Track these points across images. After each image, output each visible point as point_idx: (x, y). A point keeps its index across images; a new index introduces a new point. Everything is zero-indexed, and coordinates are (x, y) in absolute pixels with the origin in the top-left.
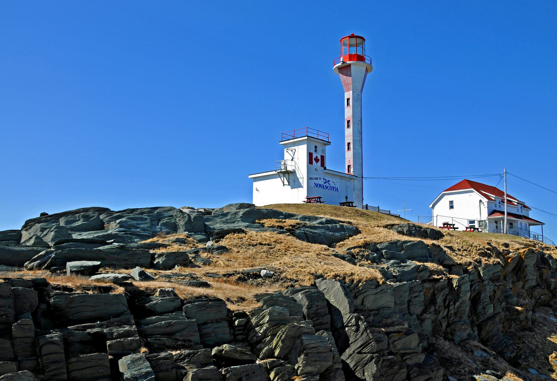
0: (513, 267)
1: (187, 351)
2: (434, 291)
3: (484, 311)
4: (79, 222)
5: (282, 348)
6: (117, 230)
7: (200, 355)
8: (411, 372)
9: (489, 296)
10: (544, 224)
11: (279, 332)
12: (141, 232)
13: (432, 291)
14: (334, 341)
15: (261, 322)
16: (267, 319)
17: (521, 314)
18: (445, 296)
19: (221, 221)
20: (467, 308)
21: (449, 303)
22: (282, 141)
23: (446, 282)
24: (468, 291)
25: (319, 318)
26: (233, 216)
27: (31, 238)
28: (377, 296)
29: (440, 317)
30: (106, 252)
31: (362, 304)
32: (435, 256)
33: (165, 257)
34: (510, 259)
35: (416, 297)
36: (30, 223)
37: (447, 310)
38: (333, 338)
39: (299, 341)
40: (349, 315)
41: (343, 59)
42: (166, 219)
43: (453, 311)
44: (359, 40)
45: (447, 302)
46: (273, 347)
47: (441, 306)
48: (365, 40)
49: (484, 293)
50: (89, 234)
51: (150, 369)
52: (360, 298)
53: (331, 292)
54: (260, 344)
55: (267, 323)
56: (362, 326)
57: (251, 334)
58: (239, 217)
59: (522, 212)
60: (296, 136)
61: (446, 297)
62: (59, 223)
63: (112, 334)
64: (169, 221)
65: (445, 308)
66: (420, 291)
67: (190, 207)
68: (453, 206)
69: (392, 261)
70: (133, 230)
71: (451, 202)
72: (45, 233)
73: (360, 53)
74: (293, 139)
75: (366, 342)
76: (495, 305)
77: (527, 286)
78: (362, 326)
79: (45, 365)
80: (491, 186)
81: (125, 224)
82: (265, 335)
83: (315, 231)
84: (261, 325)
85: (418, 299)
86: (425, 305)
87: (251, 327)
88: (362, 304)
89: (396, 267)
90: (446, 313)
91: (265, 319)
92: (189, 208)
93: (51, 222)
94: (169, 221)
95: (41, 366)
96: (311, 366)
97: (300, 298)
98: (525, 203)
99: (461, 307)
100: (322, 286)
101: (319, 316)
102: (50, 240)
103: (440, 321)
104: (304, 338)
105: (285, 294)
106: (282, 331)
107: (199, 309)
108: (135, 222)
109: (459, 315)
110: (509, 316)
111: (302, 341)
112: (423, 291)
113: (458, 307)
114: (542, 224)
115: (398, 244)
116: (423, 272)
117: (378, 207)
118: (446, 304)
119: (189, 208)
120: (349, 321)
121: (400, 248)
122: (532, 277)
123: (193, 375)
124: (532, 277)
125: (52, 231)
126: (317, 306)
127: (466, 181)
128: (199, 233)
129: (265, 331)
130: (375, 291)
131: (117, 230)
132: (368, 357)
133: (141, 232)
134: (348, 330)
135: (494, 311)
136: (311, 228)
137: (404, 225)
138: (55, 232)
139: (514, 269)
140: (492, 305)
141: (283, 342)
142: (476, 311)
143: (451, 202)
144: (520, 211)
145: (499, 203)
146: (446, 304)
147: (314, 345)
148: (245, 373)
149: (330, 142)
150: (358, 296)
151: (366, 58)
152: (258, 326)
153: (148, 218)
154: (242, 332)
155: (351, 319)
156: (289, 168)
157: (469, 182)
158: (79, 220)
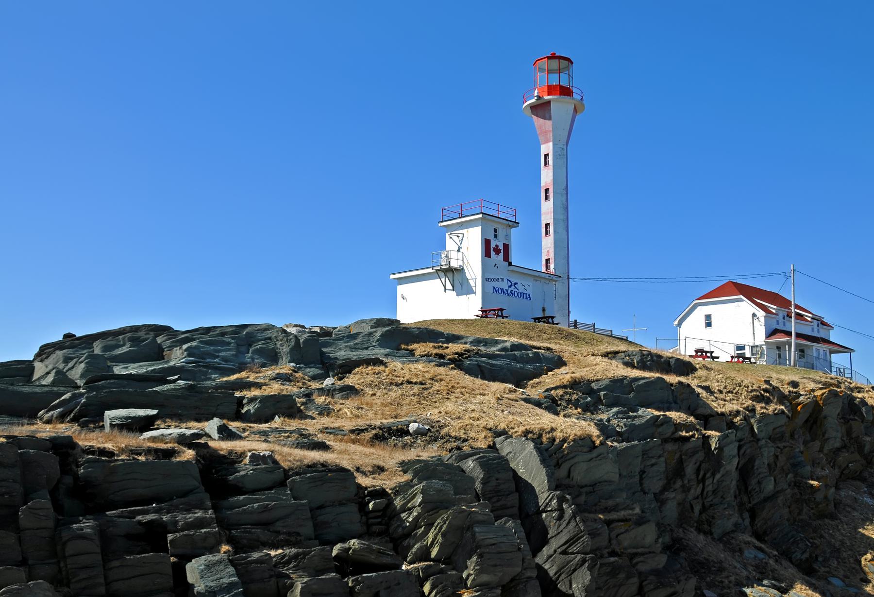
0: (805, 419)
3: (760, 487)
4: (124, 348)
5: (442, 546)
8: (644, 583)
9: (768, 464)
10: (853, 351)
11: (438, 521)
12: (221, 364)
13: (677, 456)
16: (420, 500)
18: (698, 464)
21: (705, 475)
23: (700, 443)
24: (734, 457)
25: (500, 498)
26: (366, 339)
27: (48, 373)
33: (259, 402)
34: (801, 406)
35: (652, 465)
36: (47, 349)
37: (701, 485)
39: (469, 534)
40: (548, 494)
41: (538, 93)
42: (261, 342)
44: (564, 63)
45: (702, 473)
46: (429, 544)
48: (573, 63)
50: (140, 366)
52: (565, 467)
53: (520, 457)
55: (419, 506)
56: (569, 510)
58: (376, 340)
64: (265, 346)
65: (698, 482)
66: (660, 457)
67: (298, 324)
70: (208, 360)
71: (708, 317)
72: (70, 365)
73: (564, 83)
74: (460, 218)
75: (574, 536)
78: (569, 510)
82: (416, 524)
83: (494, 362)
84: (410, 509)
87: (393, 513)
89: (621, 418)
90: (699, 490)
91: (415, 499)
92: (296, 326)
93: (80, 348)
94: (265, 346)
97: (471, 467)
98: (823, 318)
99: (723, 481)
101: (500, 496)
102: (78, 376)
104: (477, 530)
108: (212, 348)
112: (663, 456)
113: (718, 481)
114: (850, 350)
116: (664, 426)
117: (594, 325)
118: (701, 476)
119: (296, 326)
120: (548, 504)
122: (835, 434)
127: (731, 284)
128: (313, 365)
129: (416, 519)
132: (577, 559)
133: (221, 364)
134: (547, 516)
135: (775, 487)
141: (443, 535)
143: (708, 317)
146: (701, 476)
147: (492, 541)
151: (575, 90)
153: (233, 341)
154: (379, 520)
155: (551, 500)
156: (454, 264)
157: (735, 284)
158: (124, 345)
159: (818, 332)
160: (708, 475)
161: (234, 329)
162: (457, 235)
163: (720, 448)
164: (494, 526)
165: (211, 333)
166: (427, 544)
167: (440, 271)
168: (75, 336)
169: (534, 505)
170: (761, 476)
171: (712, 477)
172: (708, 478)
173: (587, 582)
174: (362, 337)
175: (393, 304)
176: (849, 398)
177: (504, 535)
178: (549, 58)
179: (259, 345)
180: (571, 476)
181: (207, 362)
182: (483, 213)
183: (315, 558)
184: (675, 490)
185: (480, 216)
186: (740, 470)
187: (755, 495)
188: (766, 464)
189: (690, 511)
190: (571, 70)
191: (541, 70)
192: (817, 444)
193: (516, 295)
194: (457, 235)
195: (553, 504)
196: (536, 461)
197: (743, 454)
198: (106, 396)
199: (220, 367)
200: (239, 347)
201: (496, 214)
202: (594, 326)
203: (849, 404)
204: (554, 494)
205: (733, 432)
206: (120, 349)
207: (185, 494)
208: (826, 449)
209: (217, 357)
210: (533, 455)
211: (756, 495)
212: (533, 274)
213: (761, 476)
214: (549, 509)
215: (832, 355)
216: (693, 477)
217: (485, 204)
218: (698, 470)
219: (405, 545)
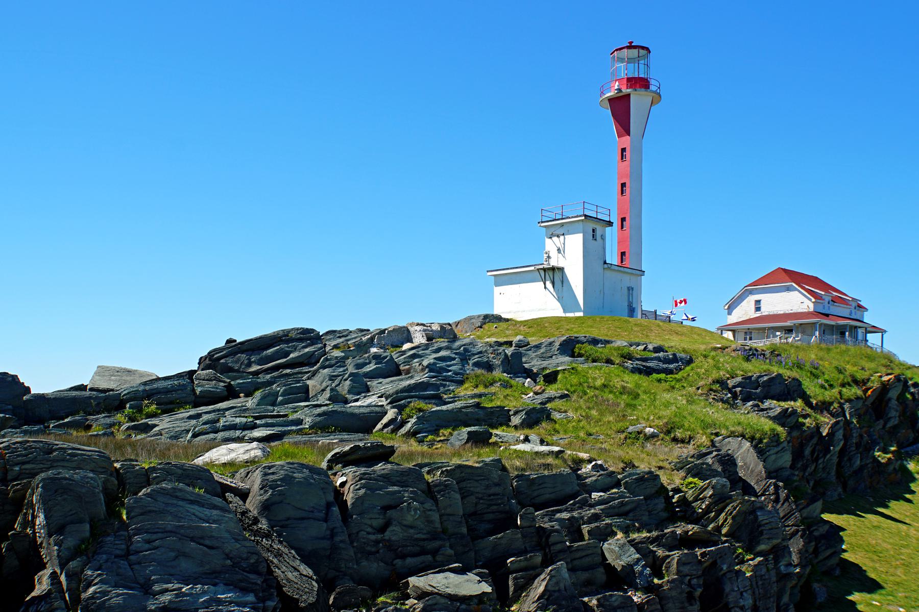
1: (654, 533)
2: (802, 440)
4: (371, 365)
5: (731, 526)
6: (426, 375)
7: (668, 537)
8: (819, 545)
10: (885, 331)
13: (799, 440)
16: (710, 493)
18: (813, 447)
19: (536, 355)
20: (835, 460)
21: (818, 455)
22: (542, 222)
23: (815, 430)
24: (841, 440)
26: (549, 348)
27: (323, 390)
28: (779, 455)
29: (807, 474)
30: (467, 414)
32: (794, 391)
33: (525, 414)
34: (871, 390)
36: (216, 354)
37: (815, 464)
39: (752, 517)
40: (765, 482)
41: (618, 86)
42: (476, 356)
43: (821, 466)
44: (642, 52)
48: (650, 52)
50: (392, 382)
51: (638, 556)
53: (738, 454)
55: (710, 497)
56: (783, 494)
58: (556, 349)
59: (855, 314)
60: (566, 214)
61: (815, 447)
62: (346, 368)
63: (582, 518)
64: (480, 359)
67: (420, 322)
68: (760, 307)
69: (751, 403)
71: (758, 302)
72: (336, 382)
74: (562, 219)
75: (788, 513)
78: (783, 494)
79: (553, 555)
80: (812, 276)
81: (434, 367)
82: (708, 510)
83: (648, 364)
84: (701, 499)
90: (813, 468)
92: (418, 324)
93: (338, 367)
94: (480, 359)
95: (549, 557)
96: (765, 544)
98: (860, 301)
99: (831, 460)
102: (346, 392)
104: (759, 514)
105: (123, 396)
107: (637, 484)
108: (444, 364)
109: (828, 470)
111: (756, 517)
113: (827, 460)
114: (883, 332)
115: (753, 379)
116: (792, 417)
117: (655, 312)
119: (418, 324)
120: (766, 489)
121: (756, 385)
122: (894, 414)
123: (678, 560)
124: (894, 414)
125: (346, 380)
128: (520, 375)
129: (708, 507)
130: (776, 450)
131: (426, 375)
132: (792, 530)
133: (454, 377)
134: (765, 499)
136: (644, 361)
137: (738, 349)
138: (350, 380)
141: (733, 518)
143: (758, 302)
144: (826, 308)
145: (829, 303)
147: (768, 521)
148: (719, 555)
151: (652, 82)
152: (697, 501)
153: (456, 356)
155: (768, 487)
157: (785, 271)
158: (370, 363)
159: (855, 314)
160: (821, 455)
163: (831, 434)
165: (430, 349)
168: (235, 341)
170: (852, 453)
173: (800, 546)
174: (546, 346)
175: (491, 303)
178: (628, 47)
179: (476, 359)
182: (586, 216)
183: (669, 538)
184: (798, 469)
185: (583, 218)
191: (621, 60)
192: (882, 422)
198: (429, 416)
202: (656, 313)
204: (771, 483)
205: (842, 420)
206: (368, 366)
207: (573, 496)
208: (889, 425)
209: (450, 371)
213: (852, 453)
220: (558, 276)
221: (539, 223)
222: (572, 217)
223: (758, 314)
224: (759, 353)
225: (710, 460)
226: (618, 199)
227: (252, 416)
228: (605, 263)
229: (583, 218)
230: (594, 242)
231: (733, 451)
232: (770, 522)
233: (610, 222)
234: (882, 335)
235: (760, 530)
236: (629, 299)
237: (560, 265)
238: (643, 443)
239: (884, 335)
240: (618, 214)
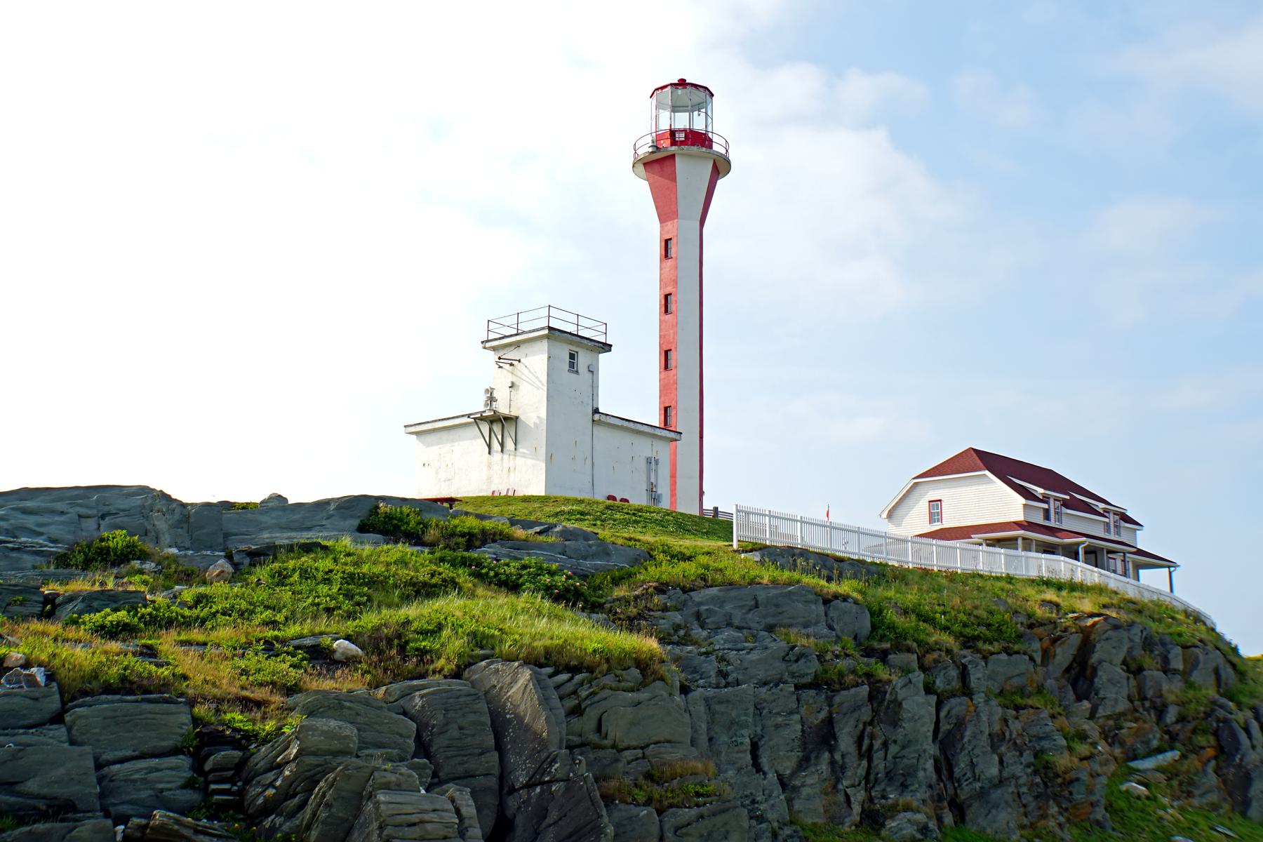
0: (1065, 665)
3: (974, 772)
9: (990, 735)
11: (322, 784)
12: (46, 546)
14: (475, 811)
15: (278, 760)
16: (295, 751)
17: (1076, 784)
25: (465, 759)
31: (599, 729)
35: (777, 727)
37: (865, 763)
38: (471, 802)
45: (866, 742)
46: (304, 823)
47: (847, 753)
49: (975, 725)
52: (591, 715)
54: (273, 816)
57: (251, 790)
60: (523, 327)
65: (861, 756)
66: (792, 713)
70: (23, 539)
71: (935, 503)
73: (699, 125)
76: (1004, 759)
77: (1101, 712)
85: (785, 732)
86: (804, 746)
87: (252, 773)
88: (599, 729)
89: (729, 649)
91: (289, 750)
97: (417, 707)
100: (488, 673)
101: (466, 756)
103: (846, 792)
106: (326, 781)
110: (1042, 786)
112: (797, 713)
113: (894, 758)
114: (1169, 564)
118: (864, 748)
126: (461, 728)
127: (972, 452)
133: (46, 546)
135: (1000, 771)
139: (1068, 670)
140: (996, 758)
142: (951, 772)
143: (935, 503)
146: (864, 748)
147: (414, 819)
149: (611, 346)
150: (586, 708)
151: (715, 138)
154: (227, 786)
156: (503, 410)
161: (82, 492)
162: (510, 362)
164: (419, 794)
166: (302, 824)
167: (481, 420)
169: (524, 773)
171: (884, 750)
172: (877, 751)
176: (1145, 633)
177: (434, 810)
180: (604, 729)
181: (21, 543)
182: (550, 328)
186: (941, 742)
187: (965, 783)
188: (987, 733)
189: (845, 805)
190: (709, 107)
193: (1063, 694)
194: (510, 362)
195: (553, 770)
196: (532, 699)
197: (946, 716)
199: (43, 551)
200: (82, 519)
201: (572, 329)
203: (1144, 643)
210: (528, 690)
211: (967, 785)
212: (633, 427)
214: (546, 779)
215: (1141, 571)
216: (852, 749)
217: (582, 321)
218: (860, 741)
219: (267, 826)
220: (510, 429)
221: (482, 342)
222: (530, 332)
223: (936, 526)
224: (601, 507)
225: (417, 700)
226: (661, 321)
227: (1167, 812)
228: (596, 411)
229: (546, 332)
230: (574, 376)
231: (501, 688)
232: (422, 822)
233: (605, 344)
234: (1170, 573)
235: (267, 823)
236: (649, 477)
237: (513, 414)
238: (210, 662)
239: (1174, 574)
240: (660, 345)
